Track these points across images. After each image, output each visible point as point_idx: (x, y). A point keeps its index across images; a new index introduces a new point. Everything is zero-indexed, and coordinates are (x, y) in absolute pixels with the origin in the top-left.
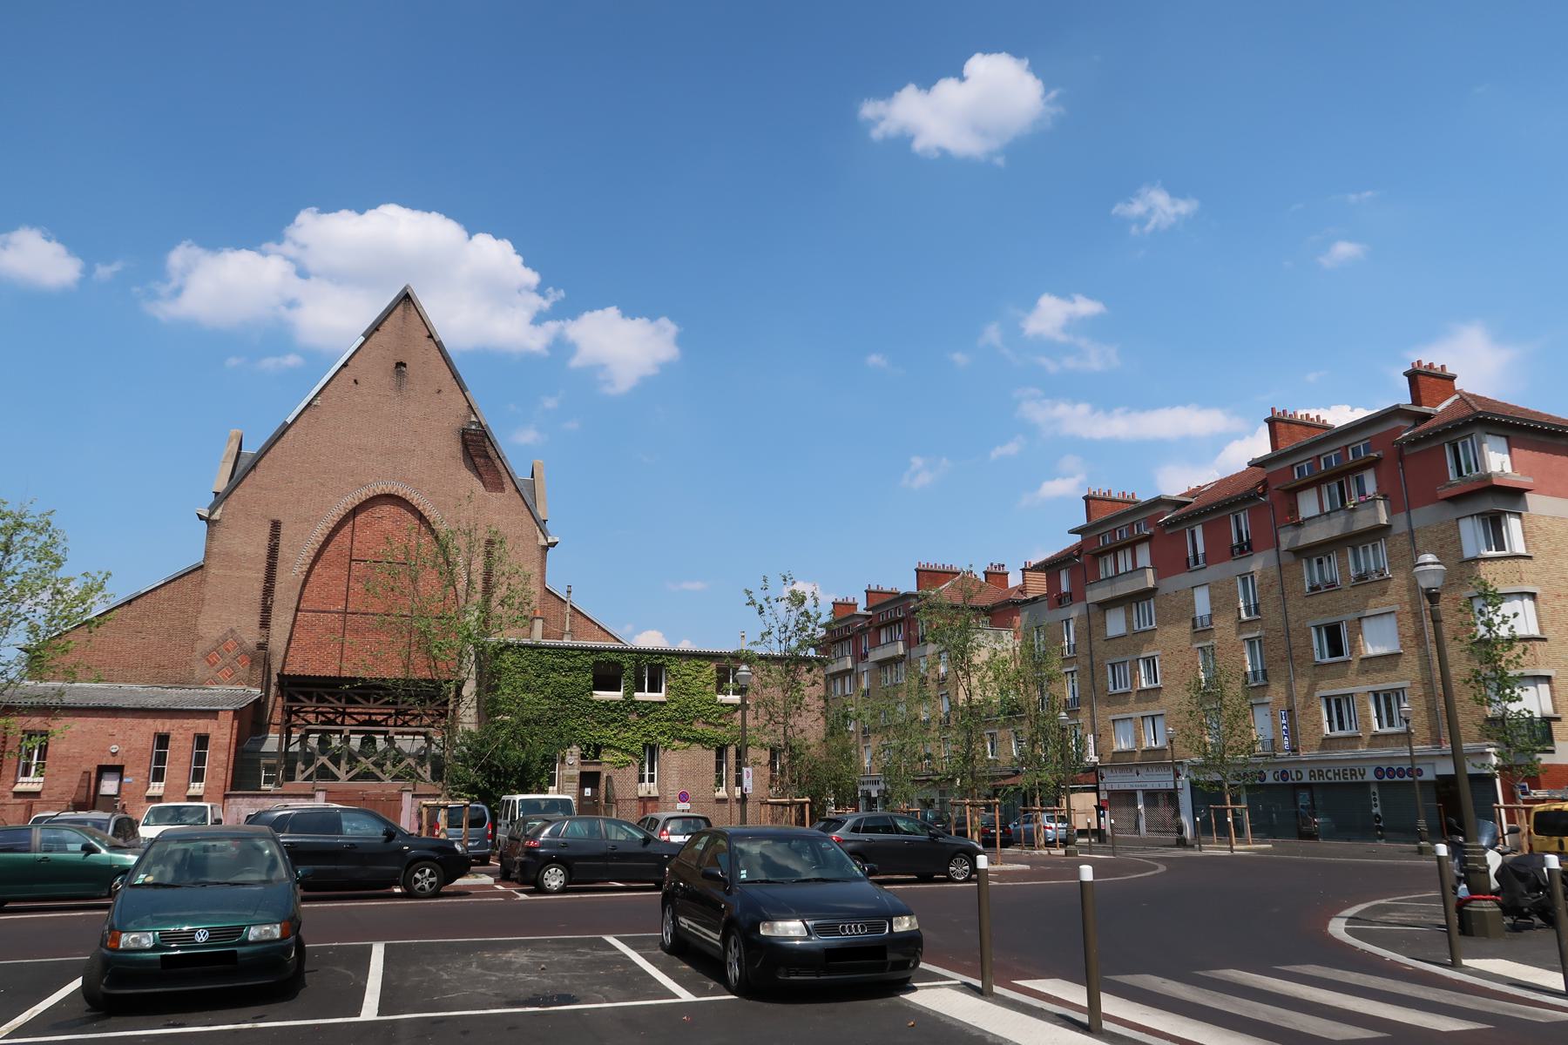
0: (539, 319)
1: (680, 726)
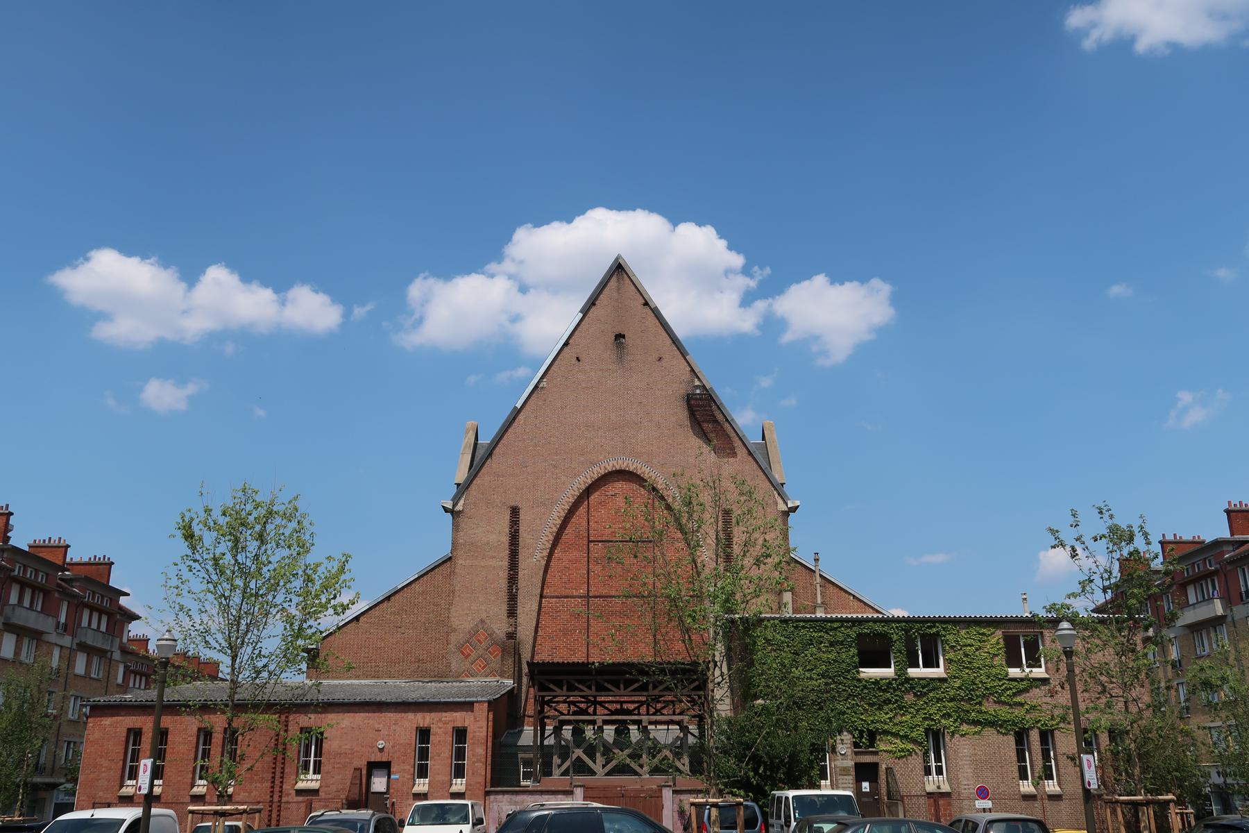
0: (747, 300)
1: (967, 707)
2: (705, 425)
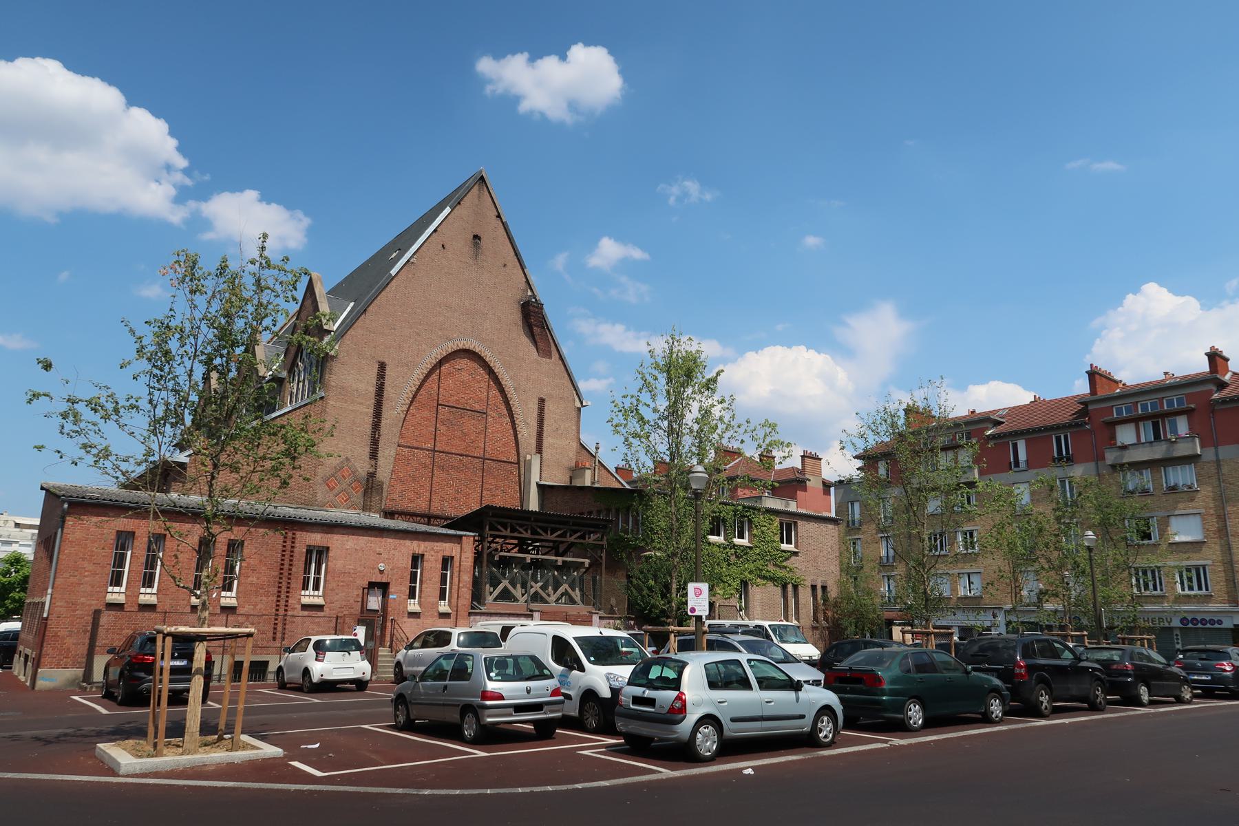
2: (535, 329)
